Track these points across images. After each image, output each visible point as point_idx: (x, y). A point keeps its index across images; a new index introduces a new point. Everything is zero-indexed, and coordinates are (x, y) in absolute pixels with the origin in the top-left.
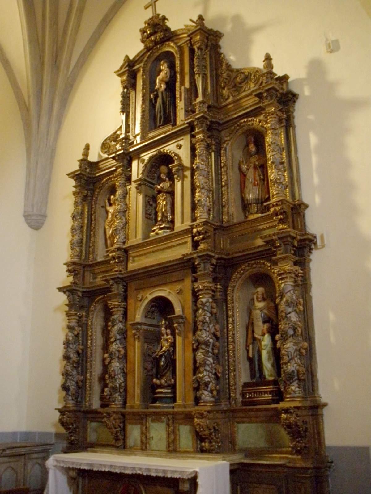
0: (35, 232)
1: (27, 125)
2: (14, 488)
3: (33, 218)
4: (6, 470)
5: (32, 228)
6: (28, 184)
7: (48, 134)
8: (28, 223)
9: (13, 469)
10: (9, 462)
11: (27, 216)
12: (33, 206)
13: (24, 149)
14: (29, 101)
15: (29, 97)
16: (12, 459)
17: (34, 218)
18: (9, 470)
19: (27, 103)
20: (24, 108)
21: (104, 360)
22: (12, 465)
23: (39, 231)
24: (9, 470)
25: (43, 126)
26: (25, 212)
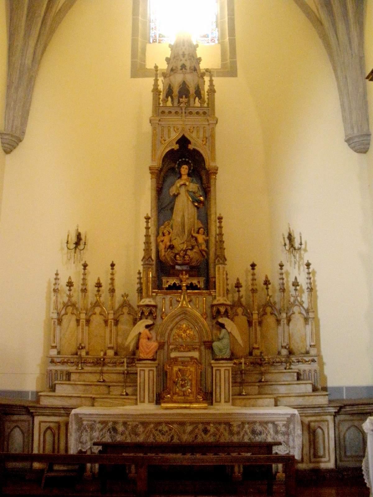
0: (363, 156)
1: (324, 38)
2: (21, 453)
3: (355, 140)
4: (349, 428)
5: (358, 152)
6: (342, 105)
7: (350, 43)
8: (352, 148)
9: (356, 427)
10: (352, 420)
11: (348, 140)
12: (352, 128)
13: (331, 68)
14: (319, 14)
15: (318, 10)
16: (355, 417)
17: (356, 140)
18: (353, 429)
19: (318, 16)
20: (317, 22)
21: (295, 261)
22: (356, 423)
23: (367, 153)
24: (57, 425)
25: (343, 37)
26: (346, 136)
